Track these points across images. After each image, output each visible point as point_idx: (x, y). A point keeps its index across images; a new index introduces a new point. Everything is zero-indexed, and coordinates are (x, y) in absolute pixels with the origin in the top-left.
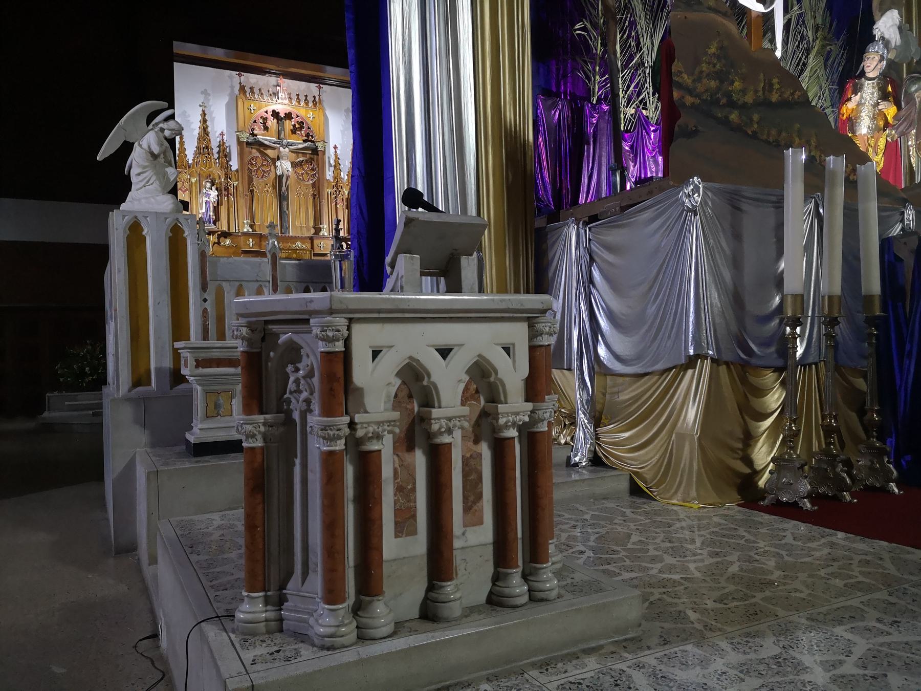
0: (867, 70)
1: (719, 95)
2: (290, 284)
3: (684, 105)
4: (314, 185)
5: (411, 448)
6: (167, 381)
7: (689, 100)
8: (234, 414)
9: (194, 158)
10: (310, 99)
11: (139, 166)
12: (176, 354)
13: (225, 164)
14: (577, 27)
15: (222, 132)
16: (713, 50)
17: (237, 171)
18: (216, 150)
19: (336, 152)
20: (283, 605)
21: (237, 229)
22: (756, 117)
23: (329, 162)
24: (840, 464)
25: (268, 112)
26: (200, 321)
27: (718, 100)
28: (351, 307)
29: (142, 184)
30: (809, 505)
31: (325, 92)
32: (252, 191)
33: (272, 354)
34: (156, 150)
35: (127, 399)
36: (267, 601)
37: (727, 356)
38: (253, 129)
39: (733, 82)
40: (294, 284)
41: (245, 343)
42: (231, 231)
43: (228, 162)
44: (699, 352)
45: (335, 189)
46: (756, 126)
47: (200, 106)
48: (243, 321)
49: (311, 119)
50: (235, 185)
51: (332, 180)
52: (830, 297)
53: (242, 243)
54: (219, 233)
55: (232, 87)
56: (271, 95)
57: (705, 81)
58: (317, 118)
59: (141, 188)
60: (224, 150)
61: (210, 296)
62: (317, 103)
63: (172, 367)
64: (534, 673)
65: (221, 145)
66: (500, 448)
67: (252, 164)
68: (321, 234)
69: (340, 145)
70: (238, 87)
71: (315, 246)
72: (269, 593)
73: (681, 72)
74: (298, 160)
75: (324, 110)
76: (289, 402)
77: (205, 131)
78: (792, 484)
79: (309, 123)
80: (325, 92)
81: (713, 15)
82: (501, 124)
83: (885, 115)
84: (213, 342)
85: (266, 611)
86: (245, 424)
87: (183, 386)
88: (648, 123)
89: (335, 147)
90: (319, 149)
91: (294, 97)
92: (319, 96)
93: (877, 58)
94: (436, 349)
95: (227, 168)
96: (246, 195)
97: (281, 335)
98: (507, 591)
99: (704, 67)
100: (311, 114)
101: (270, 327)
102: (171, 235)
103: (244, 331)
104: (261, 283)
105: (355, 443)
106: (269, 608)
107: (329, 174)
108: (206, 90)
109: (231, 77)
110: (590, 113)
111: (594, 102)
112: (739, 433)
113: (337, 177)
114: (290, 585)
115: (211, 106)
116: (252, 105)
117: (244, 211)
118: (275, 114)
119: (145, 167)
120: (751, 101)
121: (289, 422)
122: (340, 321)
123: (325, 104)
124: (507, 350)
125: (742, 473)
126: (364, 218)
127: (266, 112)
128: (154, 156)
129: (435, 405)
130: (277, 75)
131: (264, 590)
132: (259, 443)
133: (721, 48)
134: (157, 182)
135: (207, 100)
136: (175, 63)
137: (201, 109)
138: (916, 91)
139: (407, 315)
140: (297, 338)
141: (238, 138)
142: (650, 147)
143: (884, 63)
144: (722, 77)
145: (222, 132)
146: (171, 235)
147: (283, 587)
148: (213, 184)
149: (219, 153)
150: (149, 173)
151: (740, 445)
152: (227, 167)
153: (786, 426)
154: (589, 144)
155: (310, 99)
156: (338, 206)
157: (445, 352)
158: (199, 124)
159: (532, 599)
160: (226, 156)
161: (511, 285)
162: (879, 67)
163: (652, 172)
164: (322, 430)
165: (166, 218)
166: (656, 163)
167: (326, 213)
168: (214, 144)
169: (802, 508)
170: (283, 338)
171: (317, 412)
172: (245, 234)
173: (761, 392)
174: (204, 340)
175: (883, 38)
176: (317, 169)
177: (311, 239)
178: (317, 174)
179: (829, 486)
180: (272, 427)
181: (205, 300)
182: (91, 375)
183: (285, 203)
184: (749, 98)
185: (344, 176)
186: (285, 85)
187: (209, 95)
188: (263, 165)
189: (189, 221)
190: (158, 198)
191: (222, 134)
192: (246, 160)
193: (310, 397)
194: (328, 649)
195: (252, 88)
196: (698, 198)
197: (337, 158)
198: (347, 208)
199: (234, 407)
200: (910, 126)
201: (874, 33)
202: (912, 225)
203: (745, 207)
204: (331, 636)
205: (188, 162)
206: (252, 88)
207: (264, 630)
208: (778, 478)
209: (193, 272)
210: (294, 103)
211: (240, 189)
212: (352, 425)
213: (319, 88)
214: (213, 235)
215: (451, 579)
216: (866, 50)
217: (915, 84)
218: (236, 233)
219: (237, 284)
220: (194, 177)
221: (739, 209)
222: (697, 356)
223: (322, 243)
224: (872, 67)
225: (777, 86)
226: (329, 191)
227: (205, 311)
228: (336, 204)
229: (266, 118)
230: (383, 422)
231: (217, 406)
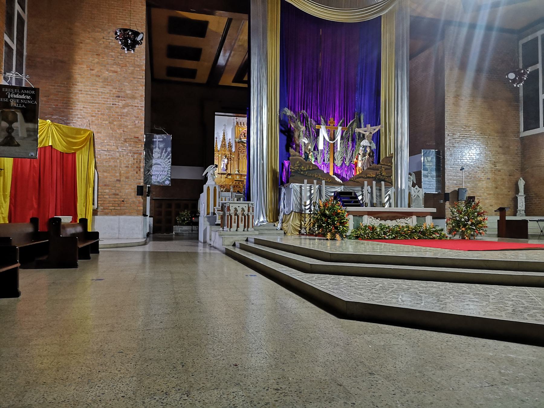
5: (235, 215)
6: (212, 214)
7: (293, 171)
12: (214, 209)
16: (298, 162)
17: (234, 152)
18: (227, 145)
32: (239, 159)
35: (206, 217)
53: (235, 177)
55: (234, 123)
60: (230, 145)
66: (245, 216)
67: (239, 149)
70: (236, 123)
77: (224, 139)
87: (215, 215)
105: (230, 214)
108: (225, 124)
109: (234, 119)
117: (236, 166)
133: (299, 162)
135: (225, 128)
148: (226, 157)
152: (230, 151)
157: (239, 207)
158: (222, 137)
172: (236, 174)
182: (187, 221)
188: (243, 149)
191: (230, 139)
192: (237, 148)
211: (235, 158)
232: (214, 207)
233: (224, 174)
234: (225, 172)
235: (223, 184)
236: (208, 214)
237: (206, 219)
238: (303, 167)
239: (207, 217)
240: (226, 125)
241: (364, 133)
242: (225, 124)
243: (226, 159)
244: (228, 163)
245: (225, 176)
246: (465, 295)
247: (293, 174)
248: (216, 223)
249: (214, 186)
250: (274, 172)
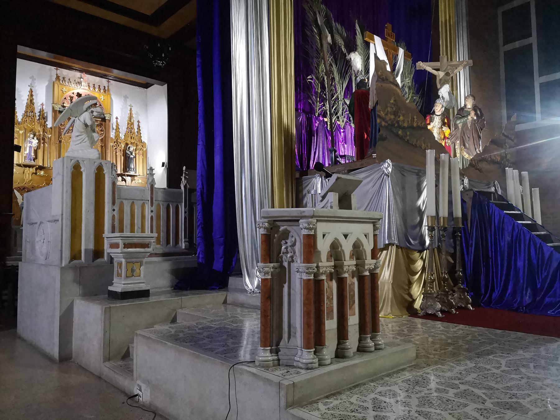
0: (436, 111)
1: (394, 122)
2: (159, 202)
3: (381, 125)
7: (383, 124)
8: (141, 275)
9: (23, 118)
10: (102, 88)
11: (78, 131)
13: (43, 124)
14: (308, 78)
15: (43, 103)
17: (51, 128)
18: (38, 114)
19: (117, 121)
20: (278, 353)
21: (49, 165)
22: (408, 133)
23: (112, 126)
24: (450, 296)
25: (74, 93)
26: (111, 222)
27: (394, 125)
28: (320, 215)
29: (79, 142)
30: (440, 315)
31: (112, 84)
32: (60, 142)
33: (276, 235)
34: (89, 123)
36: (271, 352)
37: (402, 245)
38: (64, 103)
39: (399, 117)
40: (162, 202)
41: (266, 230)
42: (45, 166)
43: (45, 122)
44: (390, 242)
45: (116, 143)
46: (408, 137)
47: (29, 86)
48: (266, 220)
49: (102, 100)
50: (49, 137)
51: (114, 138)
52: (444, 218)
54: (37, 167)
55: (51, 76)
56: (76, 83)
57: (389, 115)
58: (106, 99)
59: (78, 144)
60: (43, 114)
61: (116, 208)
62: (106, 90)
63: (94, 249)
64: (387, 378)
65: (41, 111)
69: (120, 117)
72: (273, 348)
73: (380, 111)
75: (110, 95)
76: (282, 257)
77: (31, 102)
78: (432, 305)
79: (101, 102)
80: (112, 84)
81: (392, 86)
82: (282, 126)
83: (444, 133)
84: (136, 234)
85: (272, 356)
86: (265, 267)
88: (340, 128)
89: (117, 118)
90: (107, 119)
91: (91, 85)
92: (108, 86)
93: (441, 106)
94: (343, 235)
95: (44, 126)
96: (56, 144)
97: (281, 227)
98: (367, 345)
99: (389, 109)
100: (102, 97)
101: (277, 223)
102: (96, 172)
103: (266, 224)
104: (144, 201)
106: (273, 354)
107: (112, 134)
108: (33, 76)
109: (50, 70)
110: (315, 121)
111: (317, 116)
112: (407, 282)
113: (117, 136)
114: (282, 344)
115: (36, 86)
116: (64, 88)
119: (81, 132)
120: (406, 126)
121: (282, 267)
122: (314, 220)
123: (111, 92)
124: (366, 236)
125: (409, 301)
126: (204, 167)
127: (73, 93)
128: (86, 125)
129: (342, 259)
130: (81, 71)
131: (270, 346)
132: (269, 277)
133: (395, 101)
134: (88, 141)
136: (18, 59)
137: (29, 88)
138: (459, 123)
139: (326, 219)
140: (289, 228)
141: (53, 108)
142: (341, 140)
143: (443, 109)
144: (395, 114)
145: (43, 103)
146: (96, 172)
147: (278, 344)
148: (35, 135)
149: (39, 116)
150: (84, 136)
151: (407, 288)
152: (45, 126)
153: (429, 277)
154: (314, 136)
155: (102, 88)
156: (117, 154)
157: (346, 236)
159: (376, 349)
160: (44, 118)
161: (290, 206)
162: (441, 110)
163: (342, 152)
164: (307, 269)
165: (95, 162)
166: (344, 147)
167: (109, 157)
168: (37, 111)
169: (438, 316)
170: (282, 228)
171: (299, 262)
173: (413, 262)
174: (113, 232)
175: (443, 97)
176: (104, 130)
178: (105, 133)
179: (445, 306)
180: (276, 269)
181: (114, 210)
184: (406, 125)
185: (122, 136)
186: (85, 78)
187: (35, 80)
189: (107, 164)
190: (89, 150)
191: (42, 105)
193: (294, 255)
194: (311, 369)
195: (64, 78)
196: (390, 170)
197: (117, 125)
198: (123, 156)
199: (141, 271)
200: (457, 139)
201: (439, 94)
202: (467, 186)
203: (405, 174)
204: (311, 363)
205: (18, 120)
206: (64, 78)
207: (272, 365)
208: (426, 302)
209: (108, 194)
210: (91, 89)
211: (53, 139)
212: (318, 267)
213: (108, 82)
214: (32, 168)
215: (348, 339)
216: (436, 102)
217: (459, 120)
218: (48, 167)
219: (131, 201)
220: (21, 130)
221: (404, 175)
222: (389, 244)
224: (439, 110)
225: (416, 120)
226: (112, 144)
227: (114, 216)
228: (116, 152)
229: (73, 97)
230: (328, 266)
231: (133, 271)
232: (270, 234)
233: (30, 166)
234: (32, 163)
235: (26, 185)
236: (75, 256)
237: (70, 276)
238: (401, 118)
239: (74, 268)
240: (35, 77)
241: (435, 72)
243: (35, 138)
244: (38, 147)
245: (33, 170)
246: (513, 376)
247: (383, 133)
248: (110, 288)
249: (97, 164)
250: (284, 132)
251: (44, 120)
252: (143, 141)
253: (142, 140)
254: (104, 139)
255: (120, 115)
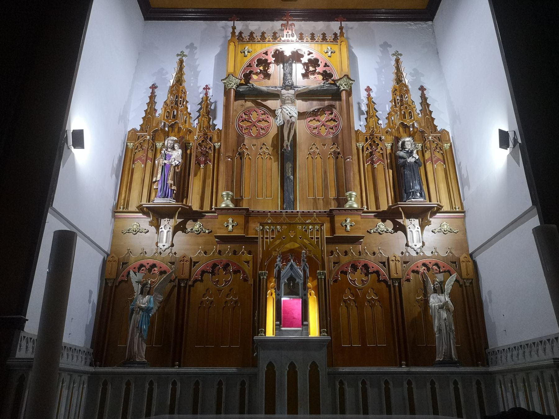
4: (335, 141)
13: (206, 123)
19: (369, 95)
23: (359, 108)
32: (241, 155)
45: (369, 142)
68: (347, 206)
71: (337, 225)
74: (311, 110)
107: (359, 124)
118: (279, 57)
177: (331, 215)
183: (289, 166)
187: (196, 48)
191: (207, 88)
223: (348, 220)
226: (360, 145)
234: (170, 202)
242: (192, 44)
251: (208, 115)
252: (439, 129)
253: (435, 127)
254: (340, 136)
255: (377, 83)
